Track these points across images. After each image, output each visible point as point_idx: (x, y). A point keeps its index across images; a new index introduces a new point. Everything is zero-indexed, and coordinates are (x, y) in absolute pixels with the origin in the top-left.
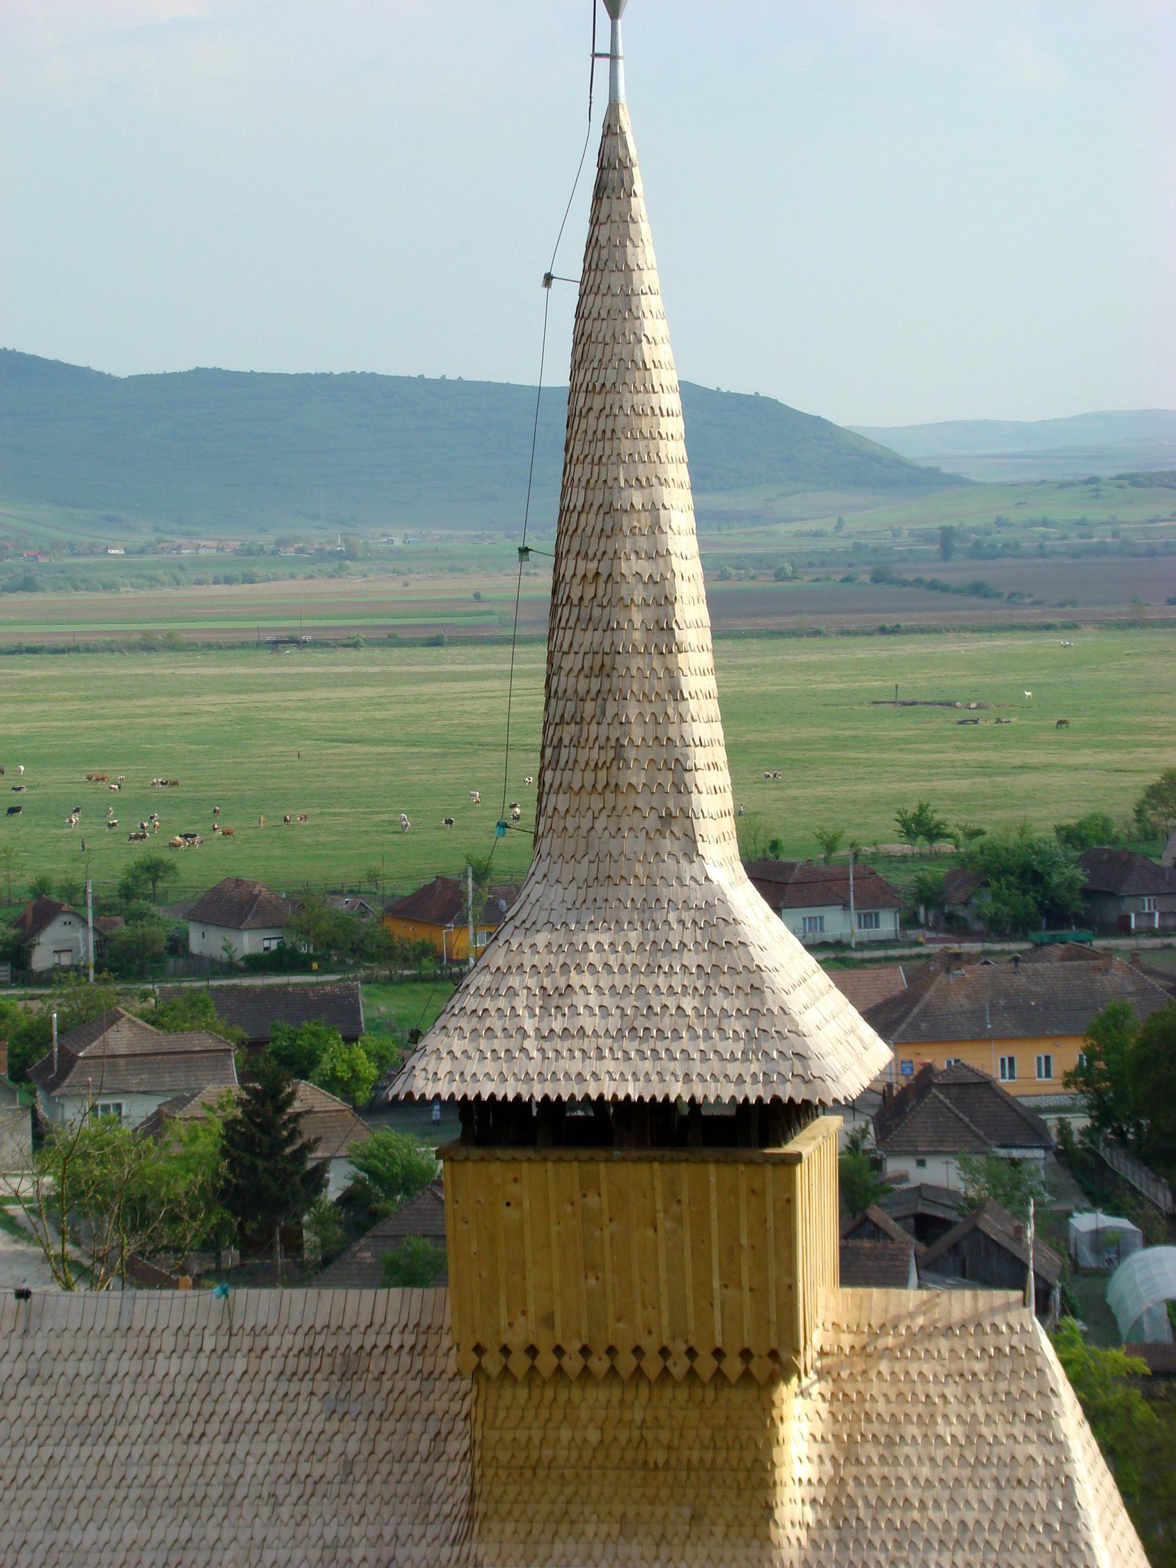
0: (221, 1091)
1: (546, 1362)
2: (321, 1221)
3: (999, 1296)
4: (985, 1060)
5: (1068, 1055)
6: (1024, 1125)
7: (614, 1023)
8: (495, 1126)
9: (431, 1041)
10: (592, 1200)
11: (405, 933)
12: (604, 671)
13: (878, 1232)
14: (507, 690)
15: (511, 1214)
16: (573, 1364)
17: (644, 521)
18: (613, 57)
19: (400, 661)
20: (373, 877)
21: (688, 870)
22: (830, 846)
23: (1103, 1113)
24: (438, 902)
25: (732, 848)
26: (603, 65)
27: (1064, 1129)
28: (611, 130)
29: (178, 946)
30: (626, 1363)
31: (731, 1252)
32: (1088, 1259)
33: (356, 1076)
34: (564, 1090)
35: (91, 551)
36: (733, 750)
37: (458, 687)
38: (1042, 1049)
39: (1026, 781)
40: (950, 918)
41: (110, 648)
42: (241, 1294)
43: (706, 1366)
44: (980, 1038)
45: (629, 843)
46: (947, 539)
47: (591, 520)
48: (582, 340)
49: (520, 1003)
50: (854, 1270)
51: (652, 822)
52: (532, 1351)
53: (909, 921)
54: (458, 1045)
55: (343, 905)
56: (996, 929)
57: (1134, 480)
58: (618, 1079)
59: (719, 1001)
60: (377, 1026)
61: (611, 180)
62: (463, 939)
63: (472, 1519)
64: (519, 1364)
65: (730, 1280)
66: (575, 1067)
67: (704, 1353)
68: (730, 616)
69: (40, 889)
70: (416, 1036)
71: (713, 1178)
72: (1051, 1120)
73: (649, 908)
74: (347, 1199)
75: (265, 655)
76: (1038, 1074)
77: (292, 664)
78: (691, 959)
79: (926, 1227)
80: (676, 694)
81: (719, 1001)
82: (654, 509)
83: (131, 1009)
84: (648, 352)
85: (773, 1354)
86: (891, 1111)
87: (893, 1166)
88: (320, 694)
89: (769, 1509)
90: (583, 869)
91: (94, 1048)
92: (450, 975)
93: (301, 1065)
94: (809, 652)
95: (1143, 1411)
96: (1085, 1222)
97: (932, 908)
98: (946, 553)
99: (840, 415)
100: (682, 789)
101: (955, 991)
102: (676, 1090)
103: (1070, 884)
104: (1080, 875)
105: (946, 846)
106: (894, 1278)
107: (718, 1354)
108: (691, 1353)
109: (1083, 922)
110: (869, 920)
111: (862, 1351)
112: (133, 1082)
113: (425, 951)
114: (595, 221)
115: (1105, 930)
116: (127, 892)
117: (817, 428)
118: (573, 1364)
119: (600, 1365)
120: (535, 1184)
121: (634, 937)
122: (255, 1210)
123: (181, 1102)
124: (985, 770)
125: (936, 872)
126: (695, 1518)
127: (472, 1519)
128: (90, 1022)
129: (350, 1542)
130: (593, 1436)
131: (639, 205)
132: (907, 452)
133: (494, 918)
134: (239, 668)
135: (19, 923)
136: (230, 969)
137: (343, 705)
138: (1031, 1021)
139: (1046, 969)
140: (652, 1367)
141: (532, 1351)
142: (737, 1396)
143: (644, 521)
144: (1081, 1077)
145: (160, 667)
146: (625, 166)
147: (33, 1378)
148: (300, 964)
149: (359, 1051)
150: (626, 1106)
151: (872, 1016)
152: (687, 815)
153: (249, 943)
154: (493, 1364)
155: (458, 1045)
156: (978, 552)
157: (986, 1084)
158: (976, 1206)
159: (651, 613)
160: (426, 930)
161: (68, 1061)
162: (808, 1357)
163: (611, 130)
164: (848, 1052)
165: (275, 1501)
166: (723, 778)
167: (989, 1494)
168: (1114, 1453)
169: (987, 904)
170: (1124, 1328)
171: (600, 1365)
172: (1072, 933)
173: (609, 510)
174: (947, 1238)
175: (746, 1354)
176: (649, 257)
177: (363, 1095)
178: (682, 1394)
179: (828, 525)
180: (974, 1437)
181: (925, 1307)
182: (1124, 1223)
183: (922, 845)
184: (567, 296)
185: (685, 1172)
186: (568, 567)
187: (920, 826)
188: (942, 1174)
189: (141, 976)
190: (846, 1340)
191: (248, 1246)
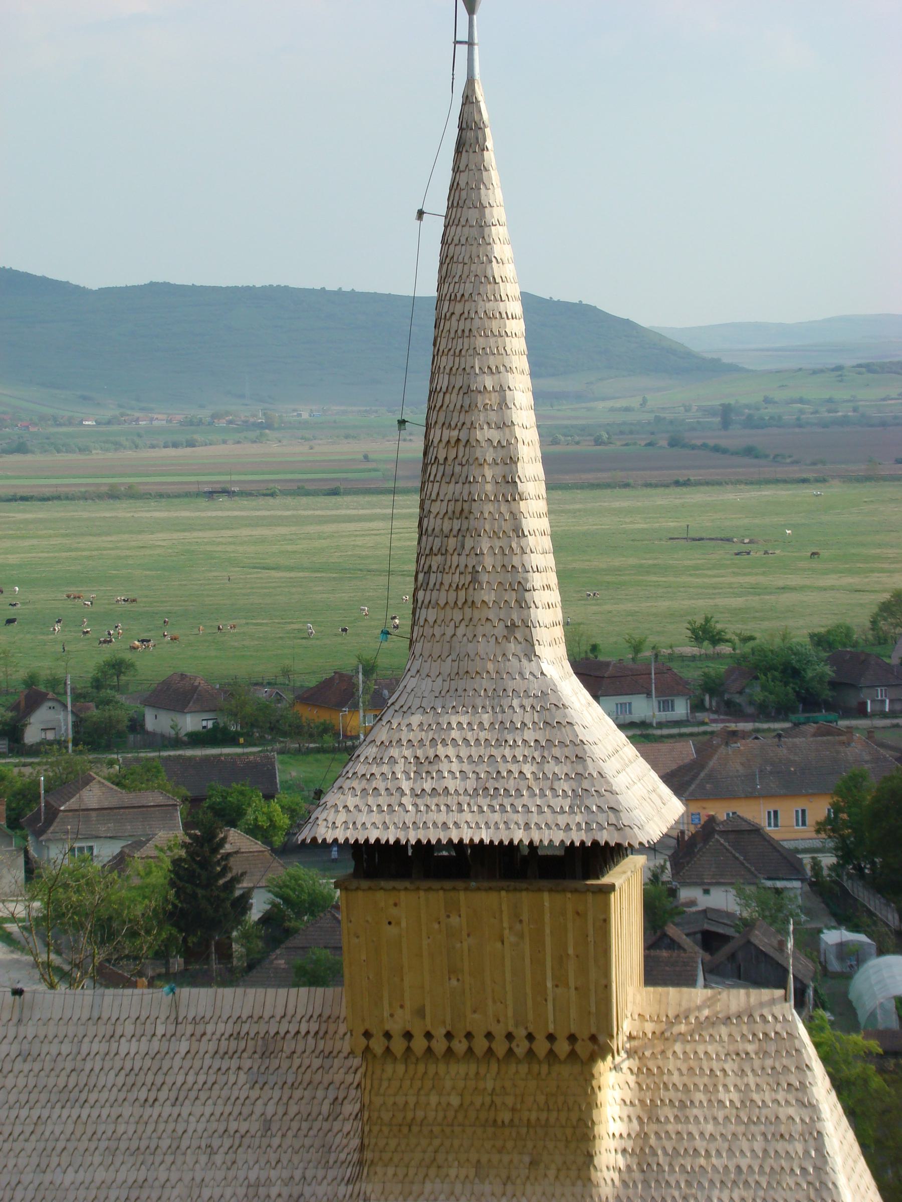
0: (169, 837)
1: (419, 1044)
2: (246, 936)
3: (766, 994)
4: (755, 813)
5: (819, 809)
6: (786, 862)
7: (471, 784)
8: (380, 863)
9: (331, 798)
10: (454, 920)
11: (311, 715)
12: (463, 514)
13: (673, 945)
14: (389, 529)
15: (393, 930)
16: (440, 1046)
17: (494, 399)
18: (470, 44)
19: (309, 507)
20: (286, 673)
21: (528, 667)
22: (637, 648)
23: (846, 853)
24: (336, 691)
25: (561, 650)
26: (462, 49)
27: (816, 866)
28: (469, 100)
29: (136, 725)
30: (480, 1045)
31: (561, 959)
32: (835, 965)
33: (273, 825)
34: (432, 836)
35: (70, 422)
36: (562, 575)
37: (351, 526)
38: (799, 804)
39: (787, 599)
40: (729, 704)
41: (85, 497)
42: (185, 992)
43: (541, 1047)
44: (751, 796)
45: (483, 647)
46: (726, 414)
47: (453, 399)
48: (446, 260)
49: (399, 769)
50: (655, 974)
51: (500, 630)
52: (408, 1036)
53: (698, 706)
54: (351, 801)
55: (263, 694)
56: (764, 712)
57: (870, 368)
58: (474, 827)
59: (552, 768)
60: (289, 787)
61: (469, 138)
62: (355, 720)
63: (362, 1165)
64: (398, 1046)
65: (560, 981)
66: (441, 818)
67: (540, 1037)
68: (560, 472)
69: (31, 682)
70: (319, 794)
71: (547, 903)
72: (806, 859)
73: (498, 696)
74: (266, 919)
75: (203, 502)
76: (796, 823)
77: (224, 509)
78: (530, 735)
79: (710, 941)
80: (519, 532)
81: (552, 768)
82: (502, 390)
83: (101, 773)
84: (497, 270)
85: (593, 1038)
86: (683, 851)
87: (685, 894)
88: (245, 532)
89: (590, 1157)
90: (447, 667)
91: (72, 803)
92: (345, 748)
93: (231, 816)
94: (620, 500)
95: (877, 1082)
96: (833, 937)
97: (714, 696)
98: (726, 424)
99: (645, 318)
100: (523, 605)
101: (732, 760)
102: (519, 836)
103: (821, 678)
104: (828, 670)
105: (725, 649)
106: (685, 980)
107: (551, 1038)
108: (530, 1037)
109: (830, 707)
110: (666, 705)
111: (661, 1036)
112: (102, 829)
113: (326, 729)
114: (456, 170)
115: (848, 713)
116: (98, 684)
117: (627, 328)
118: (440, 1046)
119: (460, 1046)
120: (410, 907)
121: (486, 718)
122: (195, 927)
123: (139, 845)
124: (755, 590)
125: (718, 668)
126: (533, 1163)
127: (362, 1165)
128: (69, 783)
129: (269, 1182)
130: (455, 1101)
131: (490, 157)
132: (696, 347)
133: (379, 704)
134: (184, 512)
135: (15, 707)
136: (176, 743)
137: (263, 540)
138: (791, 782)
139: (802, 743)
140: (500, 1048)
141: (408, 1036)
142: (565, 1070)
143: (494, 399)
144: (829, 825)
145: (123, 511)
146: (479, 128)
147: (25, 1056)
148: (230, 739)
149: (275, 806)
150: (480, 848)
151: (669, 779)
152: (527, 625)
153: (191, 723)
154: (378, 1045)
155: (351, 801)
156: (751, 423)
157: (756, 831)
158: (748, 925)
159: (499, 470)
160: (327, 714)
161: (52, 814)
162: (620, 1041)
163: (469, 100)
164: (650, 806)
165: (211, 1150)
166: (554, 596)
167: (758, 1146)
168: (854, 1114)
169: (757, 693)
170: (862, 1017)
171: (460, 1046)
172: (822, 715)
173: (467, 391)
174: (727, 949)
175: (572, 1038)
176: (497, 196)
177: (278, 840)
178: (523, 1069)
179: (635, 402)
180: (747, 1102)
181: (709, 1002)
182: (862, 938)
183: (707, 648)
184: (435, 227)
185: (526, 899)
186: (436, 434)
187: (705, 633)
188: (723, 900)
189: (108, 748)
190: (649, 1027)
191: (190, 955)
